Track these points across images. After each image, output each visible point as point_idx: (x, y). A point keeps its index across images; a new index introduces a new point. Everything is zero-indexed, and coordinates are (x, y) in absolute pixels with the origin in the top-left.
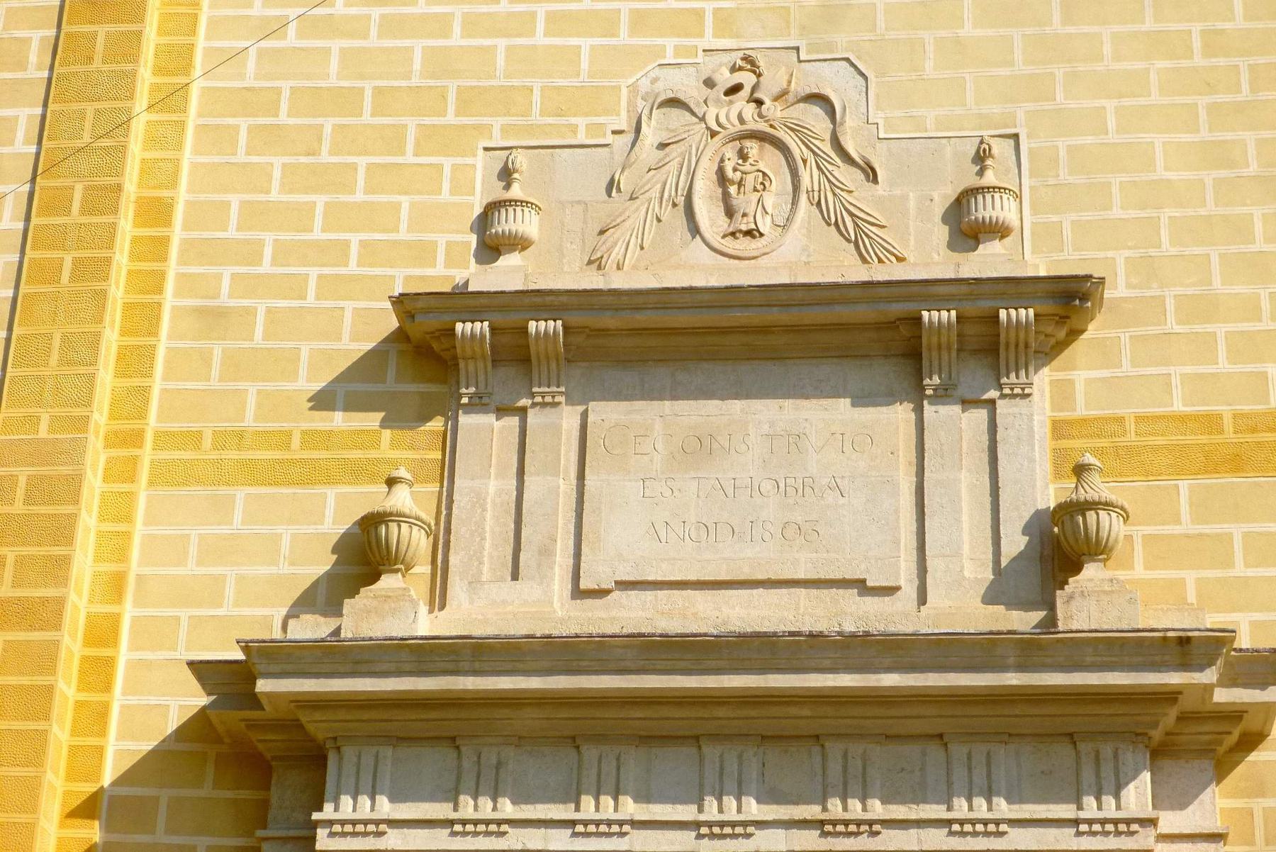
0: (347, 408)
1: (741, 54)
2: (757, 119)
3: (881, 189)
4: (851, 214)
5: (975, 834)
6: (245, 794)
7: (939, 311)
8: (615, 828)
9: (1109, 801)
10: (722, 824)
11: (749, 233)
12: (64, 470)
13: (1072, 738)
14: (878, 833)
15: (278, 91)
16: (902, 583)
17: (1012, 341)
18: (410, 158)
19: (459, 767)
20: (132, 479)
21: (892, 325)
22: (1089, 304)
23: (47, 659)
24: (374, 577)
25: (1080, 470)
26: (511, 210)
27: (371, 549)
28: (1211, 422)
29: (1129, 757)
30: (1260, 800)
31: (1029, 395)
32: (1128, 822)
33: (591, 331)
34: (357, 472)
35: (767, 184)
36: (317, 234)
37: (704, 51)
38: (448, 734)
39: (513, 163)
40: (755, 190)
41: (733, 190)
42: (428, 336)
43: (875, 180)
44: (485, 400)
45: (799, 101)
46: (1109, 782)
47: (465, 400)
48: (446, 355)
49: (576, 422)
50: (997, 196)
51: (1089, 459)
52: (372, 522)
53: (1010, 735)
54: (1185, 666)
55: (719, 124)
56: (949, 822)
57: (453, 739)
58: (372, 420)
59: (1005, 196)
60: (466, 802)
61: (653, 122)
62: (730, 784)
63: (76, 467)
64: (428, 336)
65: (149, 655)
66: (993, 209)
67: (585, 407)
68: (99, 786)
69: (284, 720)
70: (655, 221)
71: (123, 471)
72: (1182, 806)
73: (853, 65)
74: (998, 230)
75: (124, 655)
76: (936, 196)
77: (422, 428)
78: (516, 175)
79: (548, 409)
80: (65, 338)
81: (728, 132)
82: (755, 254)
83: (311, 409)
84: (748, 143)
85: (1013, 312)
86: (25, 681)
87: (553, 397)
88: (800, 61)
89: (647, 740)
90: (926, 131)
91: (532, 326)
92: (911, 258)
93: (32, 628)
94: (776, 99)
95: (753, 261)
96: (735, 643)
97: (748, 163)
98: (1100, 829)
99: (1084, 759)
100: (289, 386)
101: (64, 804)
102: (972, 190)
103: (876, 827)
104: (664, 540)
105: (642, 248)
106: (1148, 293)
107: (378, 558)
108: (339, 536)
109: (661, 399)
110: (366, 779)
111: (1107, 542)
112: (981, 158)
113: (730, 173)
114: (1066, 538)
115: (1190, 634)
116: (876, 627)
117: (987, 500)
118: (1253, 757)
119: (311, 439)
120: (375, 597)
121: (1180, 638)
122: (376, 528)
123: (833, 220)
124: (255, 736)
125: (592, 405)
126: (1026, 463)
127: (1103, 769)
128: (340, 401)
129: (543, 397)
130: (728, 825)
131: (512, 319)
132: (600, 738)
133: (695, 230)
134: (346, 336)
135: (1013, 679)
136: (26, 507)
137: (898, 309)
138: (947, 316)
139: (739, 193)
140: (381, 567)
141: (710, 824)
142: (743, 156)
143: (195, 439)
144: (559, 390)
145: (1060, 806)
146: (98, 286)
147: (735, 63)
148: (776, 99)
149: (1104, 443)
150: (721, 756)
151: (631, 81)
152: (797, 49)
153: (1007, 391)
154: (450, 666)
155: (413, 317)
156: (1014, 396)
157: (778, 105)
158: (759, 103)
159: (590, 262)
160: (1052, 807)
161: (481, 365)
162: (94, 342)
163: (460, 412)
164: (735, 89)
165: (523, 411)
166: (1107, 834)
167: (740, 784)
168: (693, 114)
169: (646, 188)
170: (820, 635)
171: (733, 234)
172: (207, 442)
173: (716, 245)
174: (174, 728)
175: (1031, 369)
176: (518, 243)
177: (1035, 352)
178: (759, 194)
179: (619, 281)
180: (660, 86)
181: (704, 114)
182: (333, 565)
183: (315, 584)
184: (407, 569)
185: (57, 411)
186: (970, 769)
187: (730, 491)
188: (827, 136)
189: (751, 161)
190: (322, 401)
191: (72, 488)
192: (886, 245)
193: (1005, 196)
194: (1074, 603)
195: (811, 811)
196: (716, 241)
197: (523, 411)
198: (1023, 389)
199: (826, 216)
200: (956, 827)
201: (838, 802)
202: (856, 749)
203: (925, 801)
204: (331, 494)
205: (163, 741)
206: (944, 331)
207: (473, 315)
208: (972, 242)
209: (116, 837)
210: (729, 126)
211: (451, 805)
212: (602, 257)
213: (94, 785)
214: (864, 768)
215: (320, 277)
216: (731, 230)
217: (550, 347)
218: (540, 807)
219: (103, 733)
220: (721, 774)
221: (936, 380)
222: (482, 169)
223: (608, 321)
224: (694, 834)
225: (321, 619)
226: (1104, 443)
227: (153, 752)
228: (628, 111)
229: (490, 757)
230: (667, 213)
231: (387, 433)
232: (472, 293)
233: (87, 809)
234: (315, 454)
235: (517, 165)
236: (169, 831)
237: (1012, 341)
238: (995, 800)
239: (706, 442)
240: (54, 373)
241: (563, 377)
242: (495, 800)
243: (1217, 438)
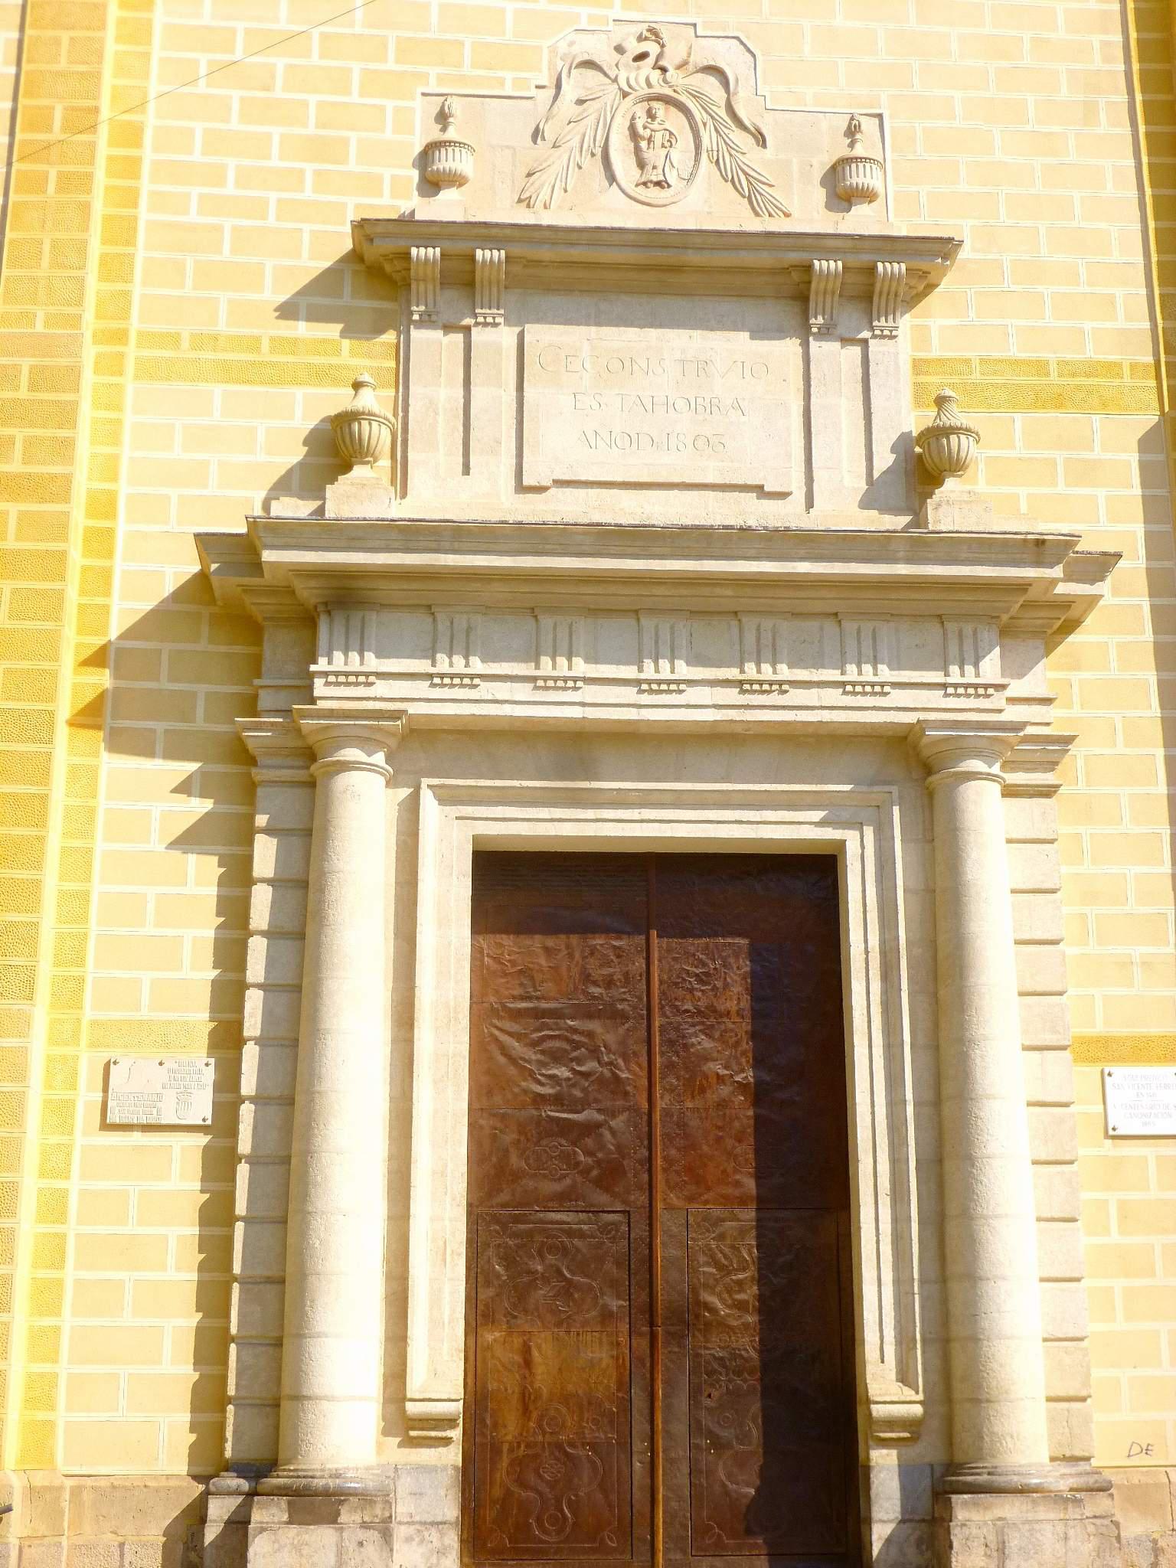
0: (310, 318)
1: (645, 26)
2: (663, 84)
3: (769, 153)
4: (746, 174)
5: (864, 694)
6: (237, 649)
7: (827, 261)
8: (570, 684)
9: (969, 669)
10: (659, 682)
11: (658, 184)
12: (63, 361)
13: (941, 619)
14: (786, 692)
15: (234, 31)
16: (793, 488)
17: (885, 289)
18: (355, 98)
19: (435, 629)
20: (120, 373)
21: (786, 270)
22: (948, 263)
23: (60, 528)
24: (347, 468)
25: (941, 401)
26: (450, 149)
27: (344, 442)
28: (1040, 367)
29: (987, 634)
30: (1076, 673)
31: (895, 337)
32: (986, 686)
33: (528, 261)
34: (322, 376)
35: (674, 142)
36: (275, 162)
37: (614, 20)
38: (424, 602)
39: (449, 109)
40: (663, 146)
41: (643, 144)
42: (381, 258)
43: (764, 145)
44: (434, 318)
45: (697, 72)
46: (969, 654)
47: (416, 317)
48: (397, 277)
49: (513, 342)
50: (868, 165)
51: (948, 392)
52: (345, 420)
53: (892, 615)
54: (1038, 564)
55: (630, 86)
56: (843, 684)
57: (429, 607)
58: (333, 330)
59: (874, 167)
60: (852, 669)
61: (572, 81)
62: (665, 649)
63: (74, 360)
64: (381, 258)
65: (143, 527)
66: (865, 176)
67: (520, 329)
68: (107, 639)
69: (278, 587)
70: (576, 168)
71: (112, 365)
72: (1021, 675)
73: (742, 43)
74: (867, 195)
75: (122, 527)
76: (815, 162)
77: (377, 340)
78: (451, 120)
79: (489, 329)
80: (55, 244)
81: (638, 94)
82: (661, 202)
83: (278, 318)
84: (655, 105)
85: (888, 265)
86: (42, 546)
87: (494, 318)
88: (697, 37)
89: (595, 612)
90: (805, 105)
91: (479, 253)
92: (795, 213)
93: (43, 500)
94: (679, 67)
95: (663, 209)
96: (679, 534)
97: (656, 122)
98: (964, 692)
99: (950, 635)
100: (255, 297)
101: (77, 653)
102: (847, 159)
103: (785, 687)
104: (593, 445)
105: (566, 191)
106: (990, 257)
107: (352, 452)
108: (308, 431)
109: (588, 324)
110: (867, 650)
111: (965, 462)
112: (852, 132)
113: (641, 130)
114: (930, 456)
115: (1046, 537)
116: (774, 523)
117: (862, 423)
118: (1071, 638)
119: (278, 344)
120: (352, 484)
121: (1037, 540)
122: (350, 425)
123: (730, 177)
124: (248, 600)
125: (527, 326)
126: (893, 394)
127: (965, 644)
128: (303, 312)
129: (485, 318)
130: (664, 683)
131: (461, 247)
132: (554, 610)
133: (611, 178)
134: (305, 254)
135: (902, 569)
136: (30, 393)
137: (794, 257)
138: (834, 266)
139: (649, 148)
140: (353, 459)
141: (649, 682)
142: (651, 115)
143: (174, 340)
144: (499, 312)
145: (931, 673)
146: (83, 198)
147: (642, 33)
148: (679, 67)
149: (956, 379)
150: (657, 627)
151: (549, 43)
152: (695, 25)
153: (877, 332)
154: (434, 545)
155: (372, 240)
156: (883, 337)
157: (681, 73)
158: (664, 70)
159: (520, 201)
160: (924, 673)
161: (430, 287)
162: (82, 248)
163: (412, 327)
164: (642, 57)
165: (467, 330)
166: (968, 696)
167: (672, 650)
168: (606, 75)
169: (568, 138)
170: (749, 529)
171: (645, 184)
172: (185, 344)
173: (633, 194)
174: (171, 591)
175: (898, 314)
176: (456, 180)
177: (902, 301)
178: (666, 150)
179: (546, 219)
180: (575, 49)
181: (617, 76)
182: (305, 456)
183: (290, 472)
184: (375, 461)
185: (52, 309)
186: (859, 642)
187: (649, 407)
188: (723, 104)
189: (658, 120)
190: (287, 311)
191: (73, 376)
192: (775, 202)
193: (874, 167)
194: (941, 510)
195: (733, 673)
196: (630, 188)
197: (865, 341)
198: (891, 331)
199: (724, 173)
200: (540, 683)
201: (854, 666)
202: (767, 623)
203: (823, 667)
204: (299, 393)
205: (162, 602)
206: (831, 279)
207: (427, 241)
208: (845, 204)
209: (123, 684)
210: (637, 88)
211: (429, 662)
212: (530, 197)
213: (103, 638)
214: (774, 639)
215: (279, 200)
216: (643, 179)
217: (429, 272)
218: (504, 664)
219: (107, 593)
220: (657, 642)
221: (820, 320)
222: (422, 112)
223: (545, 254)
224: (636, 689)
225: (301, 502)
226: (956, 379)
227: (152, 611)
228: (549, 69)
229: (461, 622)
230: (586, 161)
231: (346, 343)
232: (418, 221)
233: (98, 659)
234: (283, 358)
235: (453, 112)
236: (172, 679)
237: (885, 289)
238: (880, 666)
239: (627, 364)
240: (46, 275)
241: (502, 301)
242: (466, 658)
243: (1044, 380)
